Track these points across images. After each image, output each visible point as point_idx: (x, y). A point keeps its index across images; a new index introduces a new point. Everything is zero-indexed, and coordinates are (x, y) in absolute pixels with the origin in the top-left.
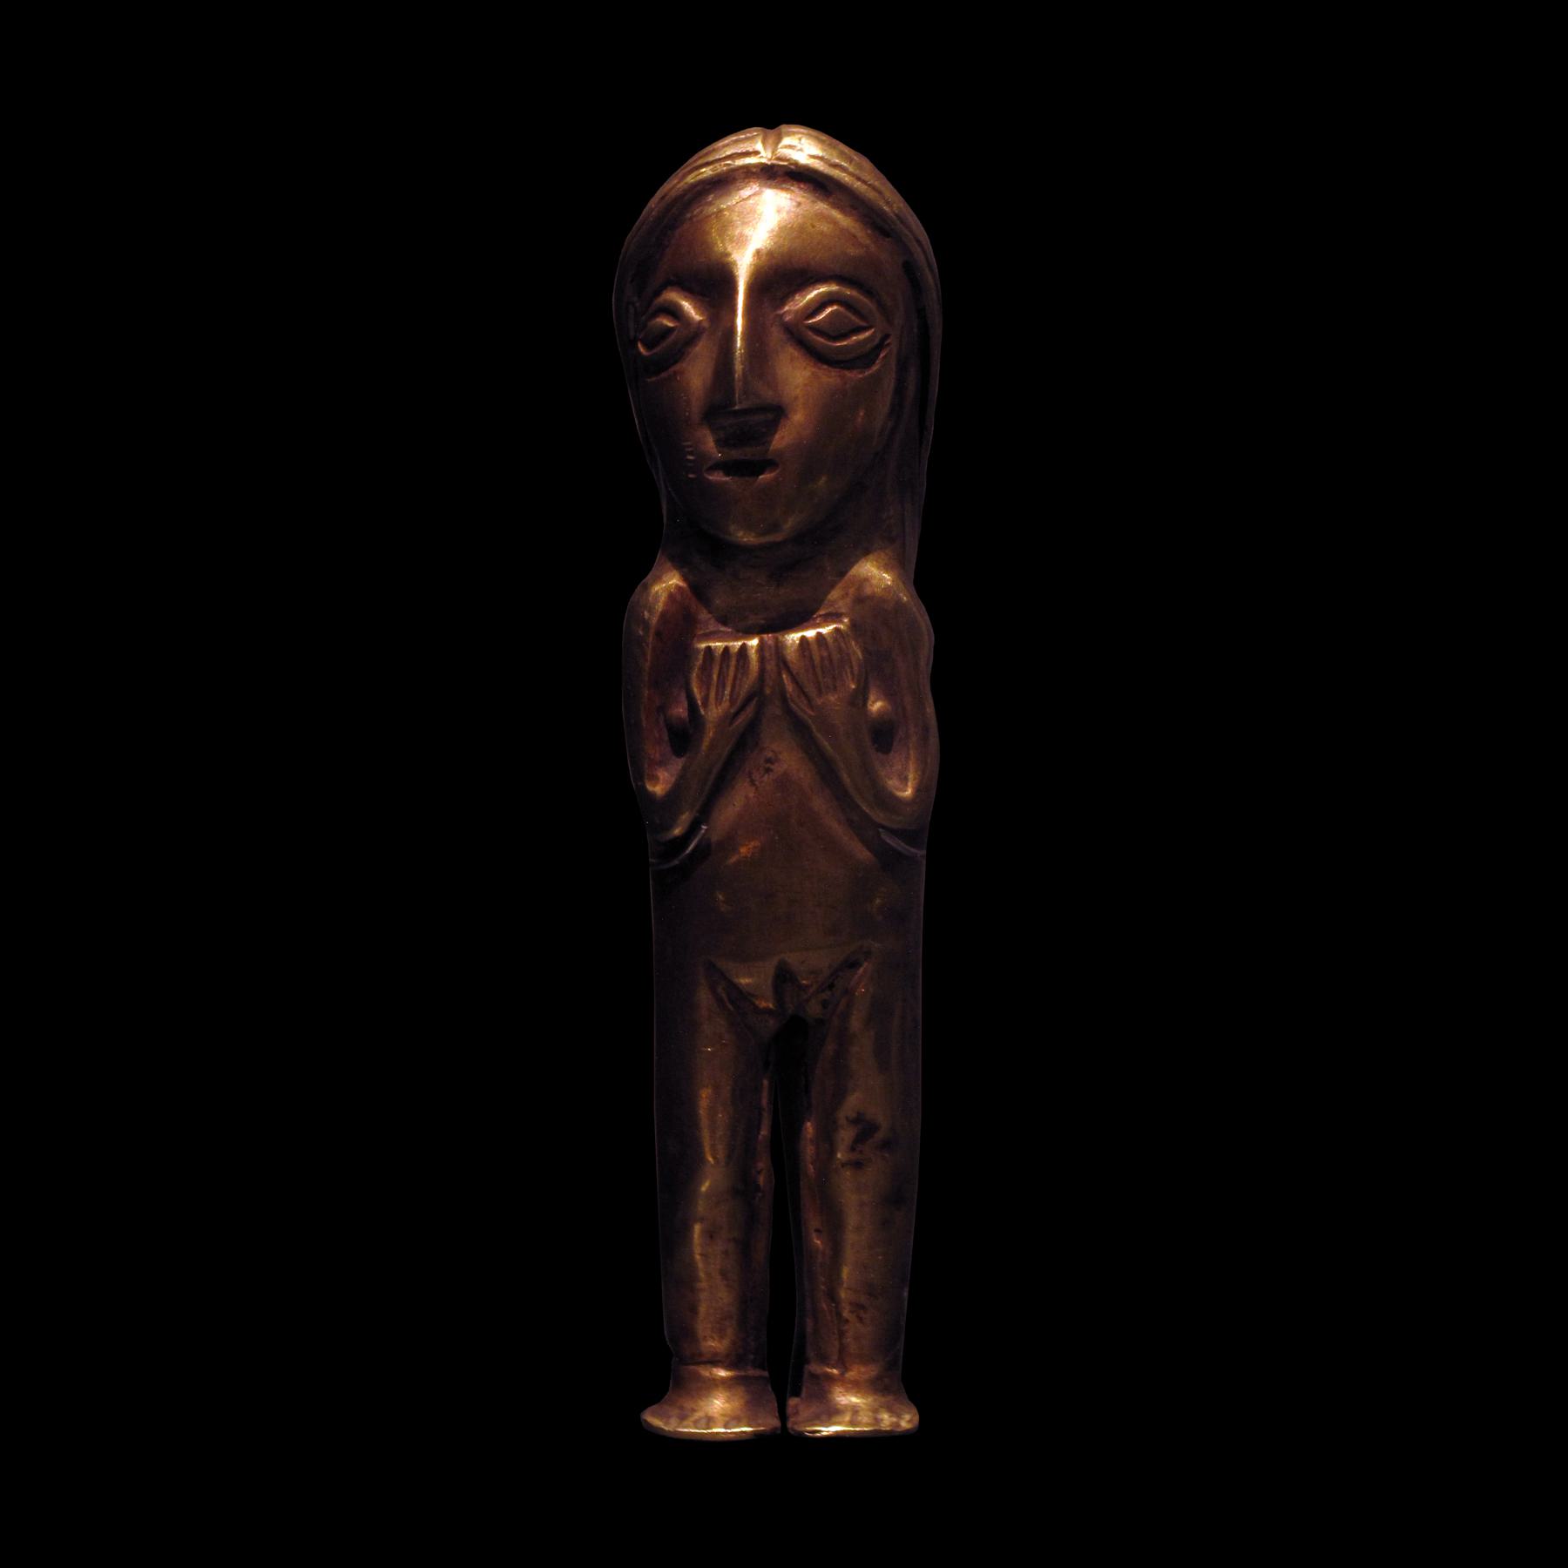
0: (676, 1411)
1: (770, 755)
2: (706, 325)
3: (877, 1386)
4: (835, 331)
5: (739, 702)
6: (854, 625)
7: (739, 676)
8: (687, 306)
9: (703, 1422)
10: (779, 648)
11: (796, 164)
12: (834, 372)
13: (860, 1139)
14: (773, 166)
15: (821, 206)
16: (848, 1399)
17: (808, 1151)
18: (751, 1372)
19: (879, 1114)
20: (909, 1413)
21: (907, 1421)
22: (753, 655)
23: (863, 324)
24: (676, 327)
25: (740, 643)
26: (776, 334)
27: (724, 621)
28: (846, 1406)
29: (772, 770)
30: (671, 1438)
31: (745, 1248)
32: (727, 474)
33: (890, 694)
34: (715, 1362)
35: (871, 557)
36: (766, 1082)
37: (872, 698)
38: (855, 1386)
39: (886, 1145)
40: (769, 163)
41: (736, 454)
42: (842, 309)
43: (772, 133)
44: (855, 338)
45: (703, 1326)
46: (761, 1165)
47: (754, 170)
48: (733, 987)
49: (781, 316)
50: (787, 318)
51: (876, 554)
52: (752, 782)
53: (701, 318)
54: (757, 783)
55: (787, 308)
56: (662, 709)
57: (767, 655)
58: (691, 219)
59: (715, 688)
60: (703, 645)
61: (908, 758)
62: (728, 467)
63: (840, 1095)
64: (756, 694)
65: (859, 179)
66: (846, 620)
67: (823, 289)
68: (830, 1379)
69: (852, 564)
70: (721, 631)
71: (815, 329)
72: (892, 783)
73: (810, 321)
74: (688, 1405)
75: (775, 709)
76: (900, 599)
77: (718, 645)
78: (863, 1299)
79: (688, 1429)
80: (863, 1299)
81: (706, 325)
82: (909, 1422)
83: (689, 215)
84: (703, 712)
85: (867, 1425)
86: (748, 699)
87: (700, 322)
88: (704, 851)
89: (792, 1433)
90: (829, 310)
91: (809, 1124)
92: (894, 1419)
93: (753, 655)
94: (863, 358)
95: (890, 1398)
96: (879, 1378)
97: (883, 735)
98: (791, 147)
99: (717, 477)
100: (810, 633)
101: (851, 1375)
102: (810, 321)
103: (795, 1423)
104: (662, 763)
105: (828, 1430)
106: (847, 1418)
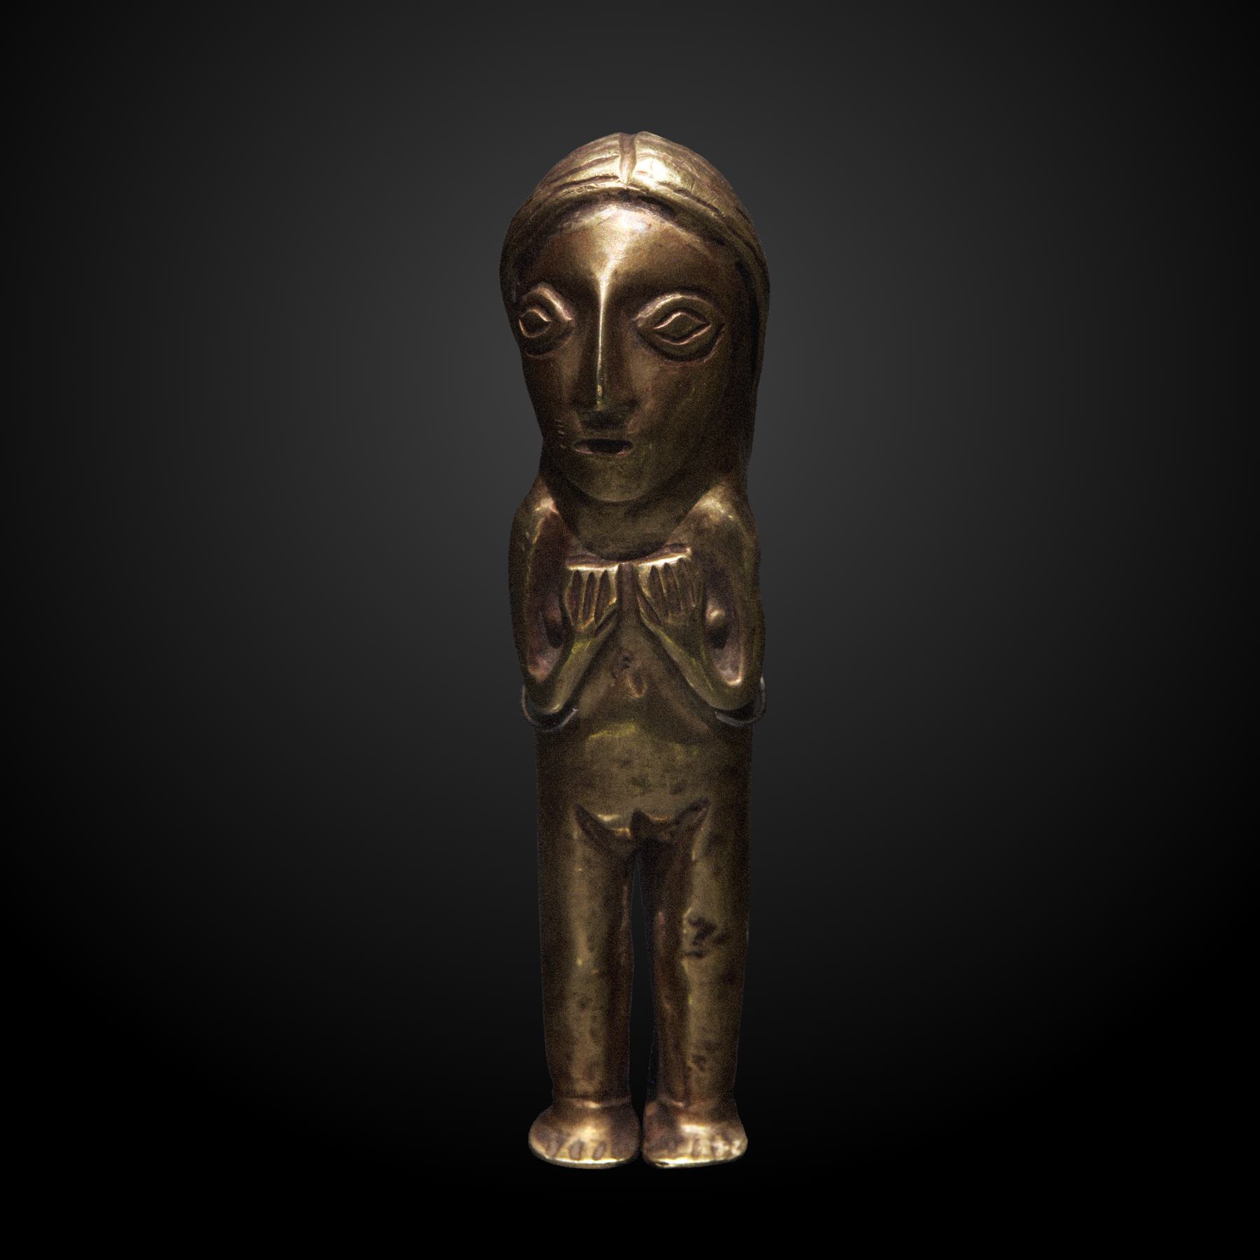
0: (554, 1135)
1: (627, 654)
2: (573, 325)
3: (715, 1117)
4: (678, 332)
5: (601, 621)
6: (695, 554)
7: (602, 596)
8: (558, 306)
9: (576, 1151)
10: (634, 574)
11: (647, 190)
12: (679, 365)
13: (700, 937)
14: (628, 191)
15: (668, 225)
16: (689, 1128)
17: (661, 937)
18: (614, 1102)
19: (715, 916)
20: (739, 1138)
21: (737, 1148)
22: (613, 579)
23: (701, 322)
24: (550, 322)
25: (602, 570)
26: (630, 338)
27: (590, 547)
29: (628, 667)
31: (610, 1013)
32: (591, 450)
33: (725, 603)
34: (586, 1097)
35: (710, 493)
36: (625, 888)
37: (710, 607)
38: (697, 1118)
39: (720, 940)
40: (625, 188)
41: (597, 435)
42: (684, 314)
43: (628, 138)
44: (695, 336)
45: (577, 1072)
47: (613, 194)
48: (598, 824)
49: (635, 323)
50: (640, 325)
51: (714, 489)
52: (613, 675)
53: (570, 319)
54: (617, 676)
55: (639, 315)
56: (542, 608)
57: (625, 579)
58: (561, 229)
59: (605, 144)
60: (572, 568)
61: (739, 650)
62: (596, 445)
63: (680, 905)
64: (618, 613)
65: (699, 200)
66: (689, 550)
67: (669, 299)
68: (679, 1111)
69: (696, 500)
70: (588, 556)
71: (663, 333)
72: (727, 672)
73: (659, 327)
74: (565, 1129)
75: (630, 621)
76: (728, 519)
77: (583, 568)
78: (703, 1053)
79: (565, 1159)
80: (703, 1053)
81: (573, 325)
82: (739, 1148)
83: (559, 226)
84: (573, 624)
85: (706, 1156)
86: (609, 618)
87: (569, 322)
88: (575, 725)
89: (645, 132)
90: (674, 316)
91: (660, 914)
92: (727, 1148)
93: (613, 579)
94: (703, 350)
95: (724, 1124)
96: (716, 1109)
99: (585, 451)
100: (660, 563)
101: (694, 1108)
102: (659, 327)
105: (672, 1162)
106: (689, 1149)
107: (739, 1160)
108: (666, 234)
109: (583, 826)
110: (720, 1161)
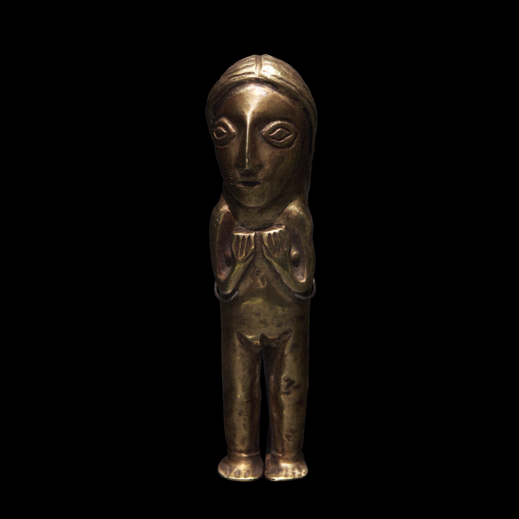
0: (228, 468)
1: (258, 270)
2: (236, 134)
3: (294, 460)
4: (279, 137)
5: (248, 256)
6: (286, 228)
7: (248, 245)
8: (230, 126)
9: (237, 474)
10: (261, 236)
11: (267, 78)
12: (280, 151)
13: (288, 386)
14: (259, 79)
15: (275, 93)
16: (284, 465)
18: (253, 454)
19: (295, 377)
20: (304, 469)
21: (303, 473)
22: (252, 239)
23: (289, 133)
24: (227, 133)
25: (248, 235)
26: (260, 139)
27: (243, 225)
28: (284, 467)
29: (259, 275)
30: (227, 480)
31: (251, 417)
32: (244, 185)
33: (298, 248)
34: (241, 452)
35: (292, 203)
36: (258, 366)
37: (292, 250)
38: (287, 460)
39: (297, 387)
40: (258, 77)
41: (246, 179)
42: (282, 129)
44: (286, 138)
45: (238, 442)
46: (256, 391)
47: (253, 80)
48: (246, 339)
49: (261, 133)
50: (264, 134)
51: (294, 202)
52: (253, 278)
53: (235, 131)
54: (254, 278)
55: (263, 130)
56: (223, 250)
57: (257, 239)
58: (231, 94)
60: (236, 234)
61: (304, 268)
62: (245, 183)
63: (280, 373)
64: (255, 252)
65: (288, 83)
66: (284, 226)
67: (276, 123)
68: (279, 458)
69: (287, 206)
70: (242, 229)
71: (273, 137)
72: (299, 277)
73: (271, 135)
74: (233, 465)
75: (259, 256)
76: (300, 214)
77: (240, 234)
78: (290, 434)
79: (233, 477)
80: (290, 434)
81: (236, 134)
82: (305, 473)
83: (230, 93)
84: (236, 257)
85: (291, 476)
86: (251, 254)
87: (234, 133)
88: (237, 299)
90: (278, 130)
91: (272, 376)
92: (299, 473)
93: (252, 239)
94: (290, 144)
95: (298, 463)
96: (295, 457)
97: (296, 262)
98: (264, 71)
99: (241, 186)
100: (272, 232)
101: (286, 456)
102: (271, 135)
103: (269, 477)
104: (223, 268)
105: (277, 479)
106: (284, 473)
107: (304, 478)
108: (274, 97)
109: (240, 340)
110: (297, 478)
